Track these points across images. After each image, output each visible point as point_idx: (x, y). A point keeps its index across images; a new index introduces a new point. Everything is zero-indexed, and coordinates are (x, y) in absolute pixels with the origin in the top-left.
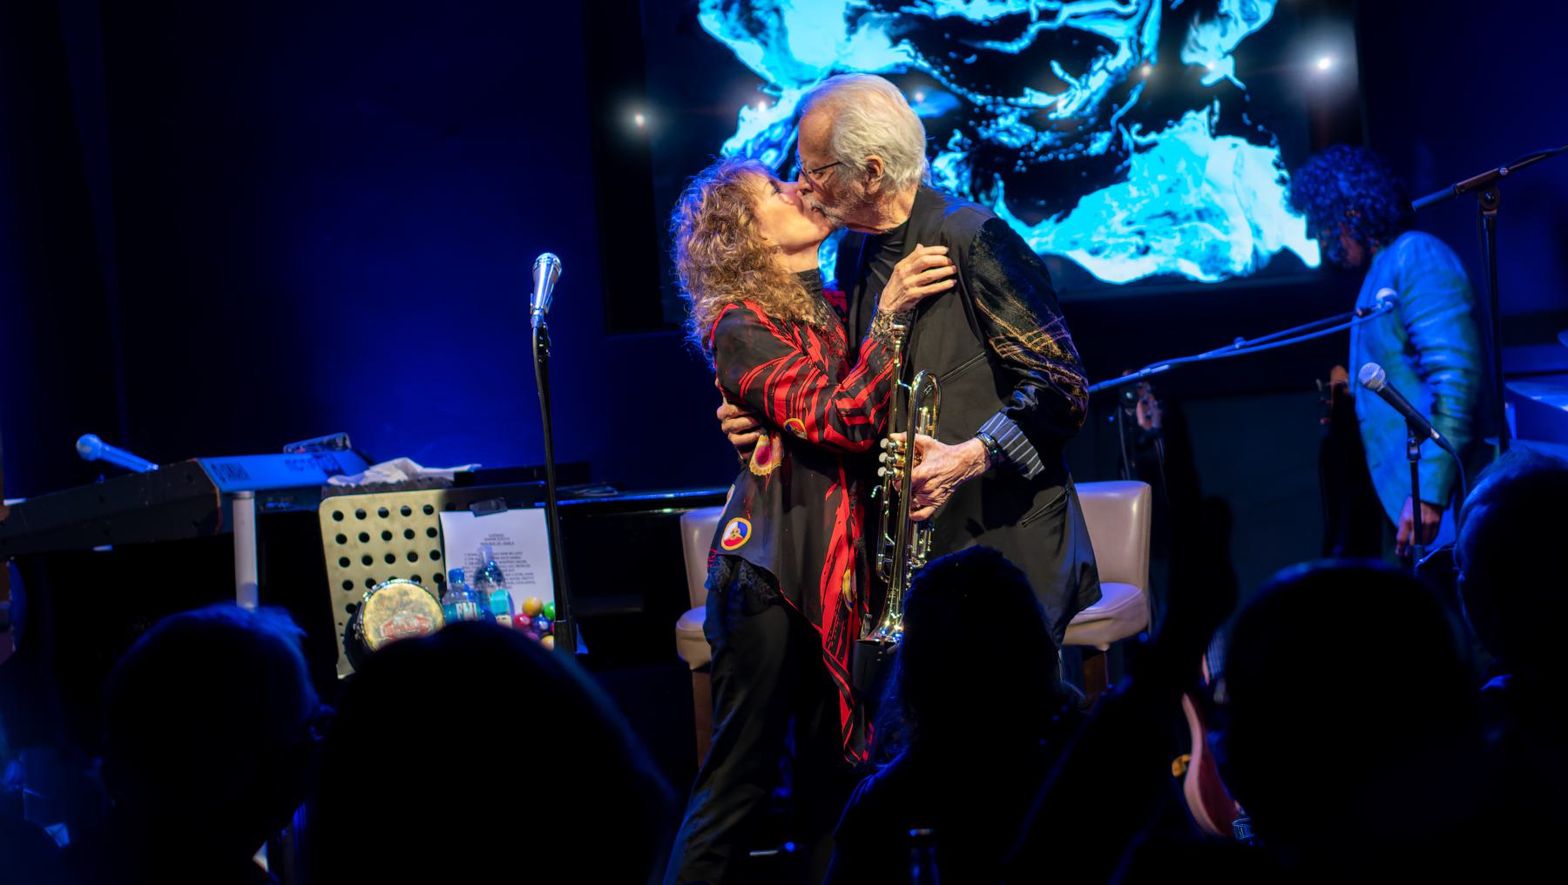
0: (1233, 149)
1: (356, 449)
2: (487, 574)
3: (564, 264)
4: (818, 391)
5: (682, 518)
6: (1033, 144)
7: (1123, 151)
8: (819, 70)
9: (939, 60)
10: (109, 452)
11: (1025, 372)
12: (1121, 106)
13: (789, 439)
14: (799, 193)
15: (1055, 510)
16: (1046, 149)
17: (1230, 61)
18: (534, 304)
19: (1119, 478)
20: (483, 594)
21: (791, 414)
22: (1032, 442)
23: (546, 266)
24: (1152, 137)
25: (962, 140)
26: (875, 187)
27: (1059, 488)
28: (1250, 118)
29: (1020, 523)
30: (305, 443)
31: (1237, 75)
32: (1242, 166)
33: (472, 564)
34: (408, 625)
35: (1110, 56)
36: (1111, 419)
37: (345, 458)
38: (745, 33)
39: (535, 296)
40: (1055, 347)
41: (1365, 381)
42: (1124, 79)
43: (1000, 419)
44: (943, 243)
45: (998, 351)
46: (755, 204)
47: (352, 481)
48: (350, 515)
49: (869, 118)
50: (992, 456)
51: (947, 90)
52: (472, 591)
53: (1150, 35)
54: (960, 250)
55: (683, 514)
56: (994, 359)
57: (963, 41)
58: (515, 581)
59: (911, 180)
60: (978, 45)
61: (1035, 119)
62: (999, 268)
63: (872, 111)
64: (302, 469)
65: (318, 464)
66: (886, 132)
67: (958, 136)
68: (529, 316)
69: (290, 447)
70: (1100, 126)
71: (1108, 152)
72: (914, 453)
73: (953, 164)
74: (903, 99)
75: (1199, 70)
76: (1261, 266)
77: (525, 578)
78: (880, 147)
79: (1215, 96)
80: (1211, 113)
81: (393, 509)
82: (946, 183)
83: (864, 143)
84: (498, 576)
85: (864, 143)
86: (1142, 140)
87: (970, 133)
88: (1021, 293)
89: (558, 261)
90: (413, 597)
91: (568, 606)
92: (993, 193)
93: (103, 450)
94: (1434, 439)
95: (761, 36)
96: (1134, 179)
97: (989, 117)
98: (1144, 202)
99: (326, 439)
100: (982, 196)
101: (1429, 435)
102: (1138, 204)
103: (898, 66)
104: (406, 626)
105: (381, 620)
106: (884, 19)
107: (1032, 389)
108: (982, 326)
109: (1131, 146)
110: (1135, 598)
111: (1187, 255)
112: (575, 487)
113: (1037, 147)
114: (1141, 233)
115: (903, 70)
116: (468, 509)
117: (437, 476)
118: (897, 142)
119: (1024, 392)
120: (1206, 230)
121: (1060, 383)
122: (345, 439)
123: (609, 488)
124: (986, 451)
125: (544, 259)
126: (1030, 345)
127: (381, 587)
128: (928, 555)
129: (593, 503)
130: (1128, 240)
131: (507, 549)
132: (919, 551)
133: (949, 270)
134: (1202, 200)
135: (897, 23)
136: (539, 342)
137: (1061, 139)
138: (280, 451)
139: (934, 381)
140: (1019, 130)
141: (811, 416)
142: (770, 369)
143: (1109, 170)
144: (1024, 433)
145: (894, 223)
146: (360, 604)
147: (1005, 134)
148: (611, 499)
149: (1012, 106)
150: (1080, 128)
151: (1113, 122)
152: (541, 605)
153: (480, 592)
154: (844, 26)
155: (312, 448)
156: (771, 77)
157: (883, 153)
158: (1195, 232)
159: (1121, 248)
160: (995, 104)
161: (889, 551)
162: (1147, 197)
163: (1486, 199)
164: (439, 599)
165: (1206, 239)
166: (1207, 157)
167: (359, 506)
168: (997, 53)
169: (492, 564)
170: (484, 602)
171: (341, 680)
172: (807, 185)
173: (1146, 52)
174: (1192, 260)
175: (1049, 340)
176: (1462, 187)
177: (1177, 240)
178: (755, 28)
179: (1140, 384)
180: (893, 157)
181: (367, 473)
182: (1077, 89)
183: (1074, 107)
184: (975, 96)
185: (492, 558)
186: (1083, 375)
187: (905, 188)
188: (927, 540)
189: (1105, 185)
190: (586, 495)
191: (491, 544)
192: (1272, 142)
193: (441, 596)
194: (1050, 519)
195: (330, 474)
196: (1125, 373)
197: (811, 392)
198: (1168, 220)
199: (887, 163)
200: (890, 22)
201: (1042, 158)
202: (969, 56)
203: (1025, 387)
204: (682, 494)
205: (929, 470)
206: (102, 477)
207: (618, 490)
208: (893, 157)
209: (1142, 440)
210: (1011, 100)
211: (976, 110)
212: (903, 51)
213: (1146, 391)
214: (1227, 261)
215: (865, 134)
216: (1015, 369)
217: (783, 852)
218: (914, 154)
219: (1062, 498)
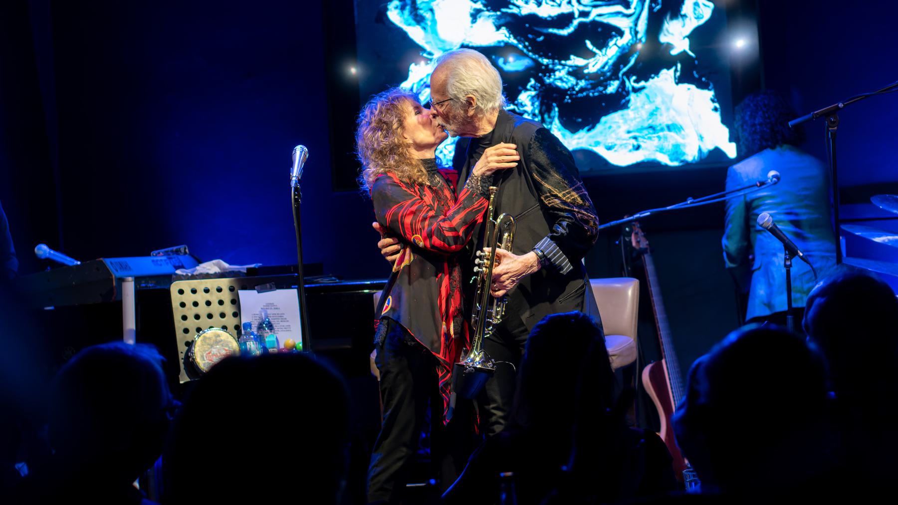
0: (689, 89)
1: (191, 254)
2: (264, 325)
3: (309, 151)
4: (428, 218)
5: (374, 295)
6: (575, 87)
7: (626, 92)
8: (454, 44)
9: (522, 39)
10: (54, 255)
11: (562, 213)
12: (625, 66)
13: (415, 248)
14: (431, 116)
15: (578, 294)
16: (582, 90)
17: (687, 41)
18: (293, 174)
19: (622, 276)
20: (262, 337)
21: (414, 232)
22: (564, 253)
23: (299, 153)
24: (642, 83)
25: (535, 84)
26: (471, 112)
27: (581, 280)
28: (697, 73)
29: (557, 300)
30: (163, 250)
31: (691, 49)
32: (693, 101)
33: (256, 320)
34: (220, 353)
35: (619, 38)
36: (617, 242)
37: (185, 259)
38: (413, 22)
39: (293, 169)
40: (579, 199)
41: (761, 223)
42: (627, 51)
43: (546, 240)
44: (513, 142)
45: (547, 203)
46: (405, 118)
47: (189, 272)
48: (187, 291)
49: (467, 74)
50: (541, 261)
51: (527, 56)
52: (256, 335)
53: (642, 26)
54: (523, 145)
55: (375, 293)
56: (544, 207)
57: (536, 29)
58: (279, 330)
59: (493, 109)
60: (545, 31)
61: (577, 73)
62: (545, 156)
63: (469, 70)
64: (161, 265)
65: (171, 263)
66: (478, 83)
67: (533, 82)
68: (290, 180)
69: (154, 253)
70: (613, 77)
71: (617, 91)
72: (496, 259)
73: (530, 97)
74: (488, 63)
75: (669, 46)
76: (703, 157)
77: (285, 328)
78: (474, 90)
79: (678, 62)
80: (676, 71)
81: (212, 288)
82: (525, 108)
83: (465, 88)
84: (270, 327)
85: (464, 88)
86: (637, 86)
87: (539, 80)
88: (559, 169)
89: (307, 150)
90: (222, 338)
91: (310, 344)
92: (552, 114)
93: (50, 253)
94: (799, 256)
95: (423, 24)
96: (632, 107)
97: (550, 71)
98: (638, 120)
99: (174, 248)
100: (546, 116)
101: (797, 254)
102: (634, 122)
103: (499, 42)
104: (218, 354)
105: (205, 351)
106: (492, 16)
107: (565, 223)
108: (537, 189)
109: (630, 89)
110: (628, 344)
111: (661, 150)
112: (314, 277)
113: (577, 89)
114: (635, 138)
115: (502, 44)
116: (254, 289)
117: (237, 270)
118: (482, 86)
119: (560, 225)
120: (671, 136)
121: (582, 219)
122: (185, 249)
123: (333, 278)
124: (538, 259)
125: (299, 148)
126: (564, 199)
127: (205, 332)
128: (502, 317)
129: (324, 286)
130: (628, 142)
131: (276, 311)
132: (497, 314)
133: (517, 158)
134: (670, 120)
135: (499, 18)
136: (295, 195)
137: (591, 84)
138: (149, 255)
139: (512, 219)
140: (567, 79)
141: (424, 233)
142: (402, 207)
143: (618, 102)
144: (560, 248)
145: (485, 131)
146: (193, 341)
147: (559, 81)
148: (335, 284)
149: (564, 65)
150: (602, 78)
151: (620, 75)
152: (295, 343)
153: (260, 336)
154: (470, 19)
155: (166, 254)
156: (428, 48)
157: (476, 94)
158: (666, 138)
159: (625, 146)
160: (554, 64)
161: (478, 313)
162: (639, 118)
163: (831, 121)
164: (237, 339)
165: (673, 142)
166: (673, 96)
167: (193, 287)
168: (555, 35)
169: (267, 320)
170: (262, 341)
171: (182, 384)
172: (435, 112)
173: (639, 36)
174: (664, 153)
175: (575, 195)
176: (817, 114)
177: (656, 142)
178: (419, 19)
179: (634, 223)
180: (482, 96)
181: (198, 268)
182: (600, 56)
183: (598, 66)
184: (542, 60)
185: (267, 317)
186: (596, 215)
187: (489, 113)
188: (503, 307)
189: (615, 110)
190: (321, 281)
191: (266, 309)
192: (710, 88)
193: (238, 338)
194: (576, 298)
195: (177, 268)
196: (625, 217)
197: (425, 219)
198: (651, 131)
199: (478, 99)
200: (495, 17)
201: (580, 95)
202: (540, 37)
203: (561, 222)
204: (375, 282)
205: (503, 269)
206: (49, 268)
207: (339, 279)
208: (482, 96)
209: (634, 255)
210: (563, 62)
211: (543, 67)
212: (503, 34)
213: (637, 228)
214: (684, 154)
215: (465, 83)
216: (556, 212)
217: (429, 484)
218: (494, 94)
219: (583, 287)
